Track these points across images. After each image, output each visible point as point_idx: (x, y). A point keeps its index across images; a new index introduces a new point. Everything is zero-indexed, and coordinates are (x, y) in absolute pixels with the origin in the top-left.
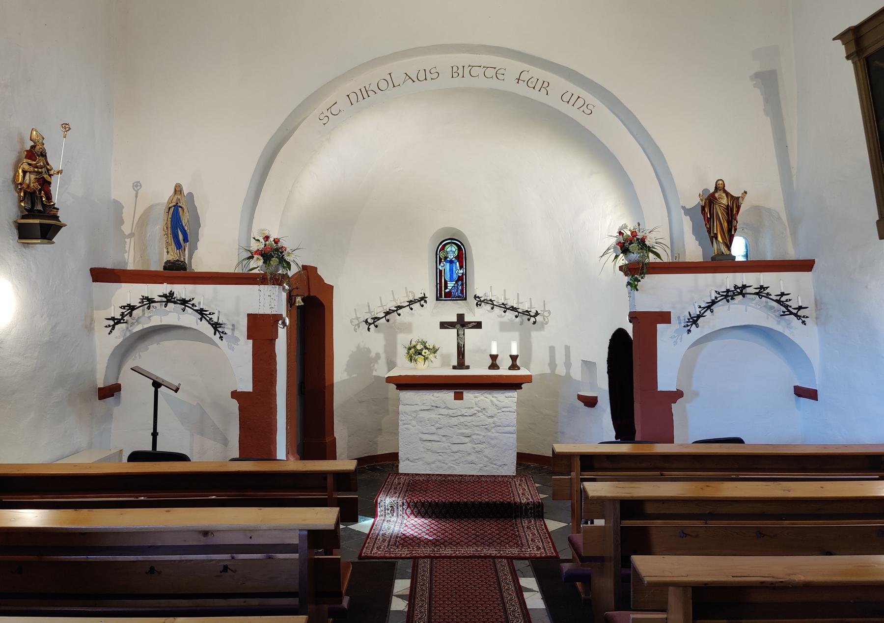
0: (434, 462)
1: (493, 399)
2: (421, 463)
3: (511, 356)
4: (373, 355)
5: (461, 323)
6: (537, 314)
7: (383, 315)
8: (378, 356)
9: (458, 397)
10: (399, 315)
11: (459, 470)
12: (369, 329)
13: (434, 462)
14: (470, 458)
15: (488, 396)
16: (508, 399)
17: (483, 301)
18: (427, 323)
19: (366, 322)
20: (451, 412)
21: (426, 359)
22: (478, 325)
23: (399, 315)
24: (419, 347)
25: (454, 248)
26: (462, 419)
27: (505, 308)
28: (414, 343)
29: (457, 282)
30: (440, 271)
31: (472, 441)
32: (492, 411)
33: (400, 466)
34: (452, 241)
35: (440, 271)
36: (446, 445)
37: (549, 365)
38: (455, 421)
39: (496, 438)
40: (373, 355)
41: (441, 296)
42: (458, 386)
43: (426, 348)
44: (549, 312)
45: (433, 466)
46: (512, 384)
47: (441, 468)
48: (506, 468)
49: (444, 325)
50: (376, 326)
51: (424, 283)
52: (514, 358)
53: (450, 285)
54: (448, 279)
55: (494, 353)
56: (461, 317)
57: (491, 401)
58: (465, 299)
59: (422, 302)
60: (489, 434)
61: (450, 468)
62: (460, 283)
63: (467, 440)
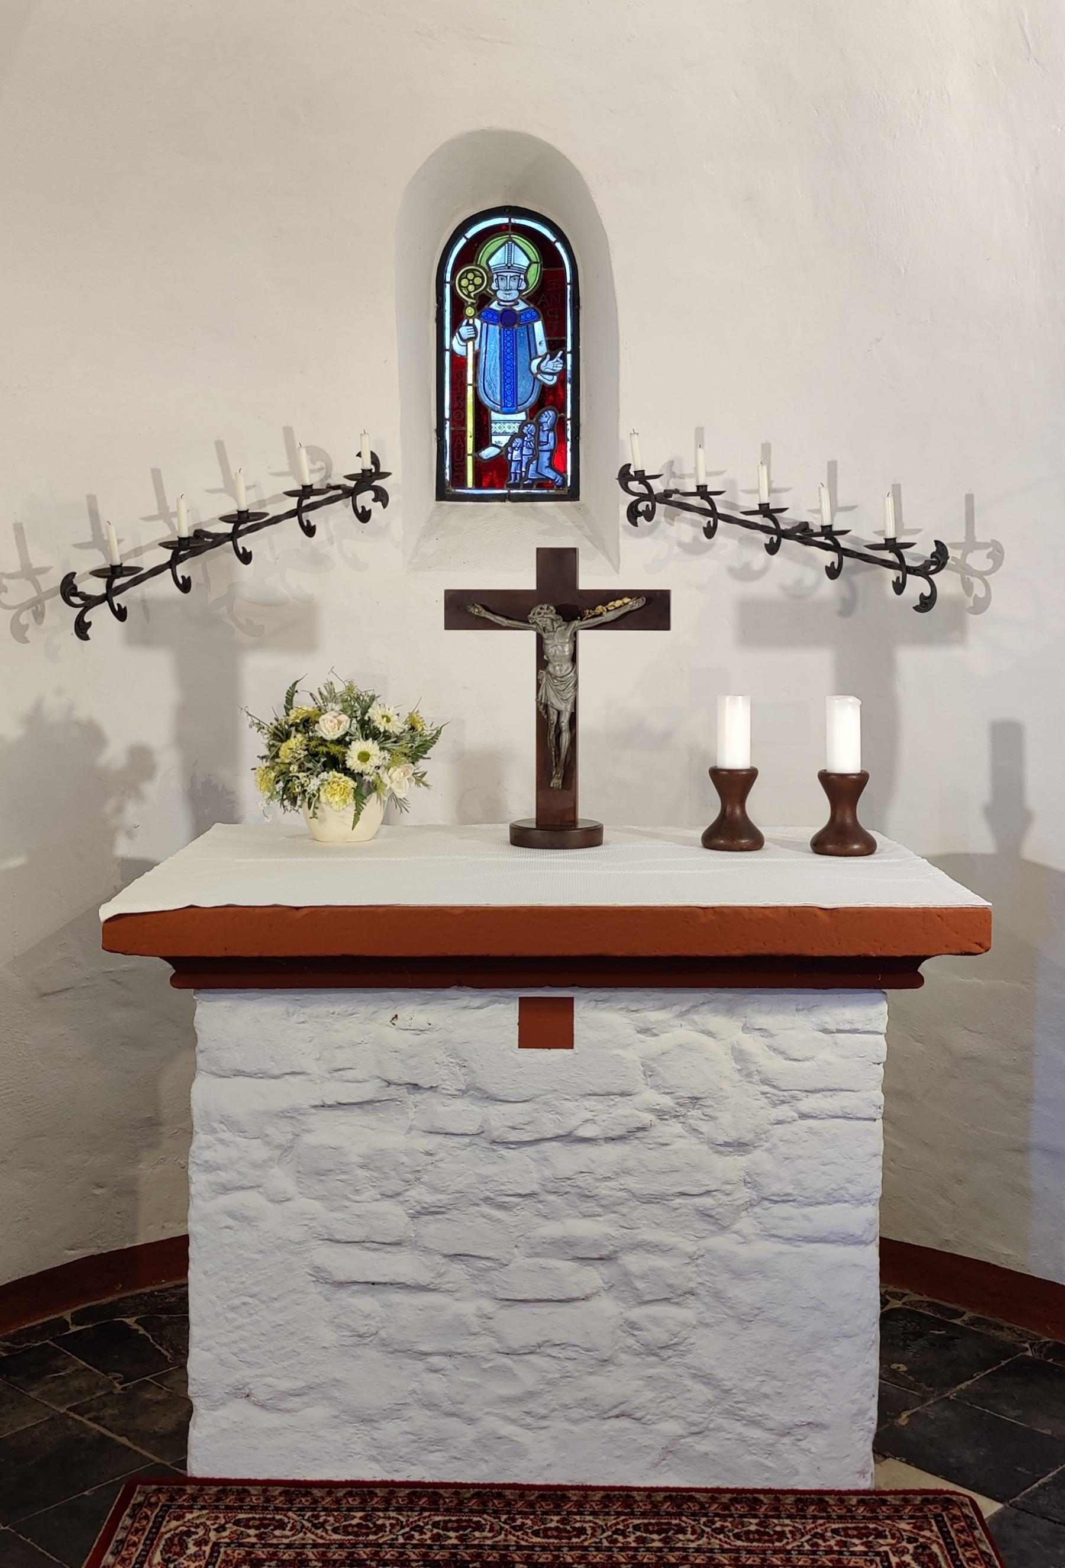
0: (394, 1412)
1: (752, 1043)
2: (318, 1412)
3: (827, 779)
4: (114, 755)
5: (559, 600)
6: (940, 556)
7: (167, 555)
8: (141, 761)
9: (547, 1028)
10: (246, 557)
11: (542, 1458)
12: (82, 629)
13: (394, 1412)
14: (607, 1386)
15: (717, 1021)
16: (842, 1040)
17: (665, 497)
18: (381, 606)
19: (68, 588)
20: (499, 1118)
21: (364, 788)
22: (651, 610)
23: (246, 557)
24: (331, 726)
25: (523, 256)
26: (566, 1161)
27: (775, 529)
28: (304, 705)
29: (534, 412)
30: (458, 363)
31: (624, 1287)
32: (742, 1109)
33: (195, 1434)
34: (515, 220)
35: (458, 363)
36: (468, 1308)
37: (990, 812)
38: (520, 1170)
39: (759, 1269)
40: (114, 755)
41: (459, 478)
42: (546, 967)
43: (368, 730)
44: (997, 553)
45: (391, 1430)
46: (863, 959)
47: (440, 1443)
48: (816, 1442)
49: (466, 610)
50: (121, 614)
51: (377, 399)
52: (843, 790)
53: (505, 426)
54: (492, 396)
55: (735, 757)
56: (556, 565)
57: (740, 1055)
58: (573, 494)
59: (366, 499)
60: (723, 1243)
61: (489, 1442)
62: (548, 417)
63: (593, 1277)
